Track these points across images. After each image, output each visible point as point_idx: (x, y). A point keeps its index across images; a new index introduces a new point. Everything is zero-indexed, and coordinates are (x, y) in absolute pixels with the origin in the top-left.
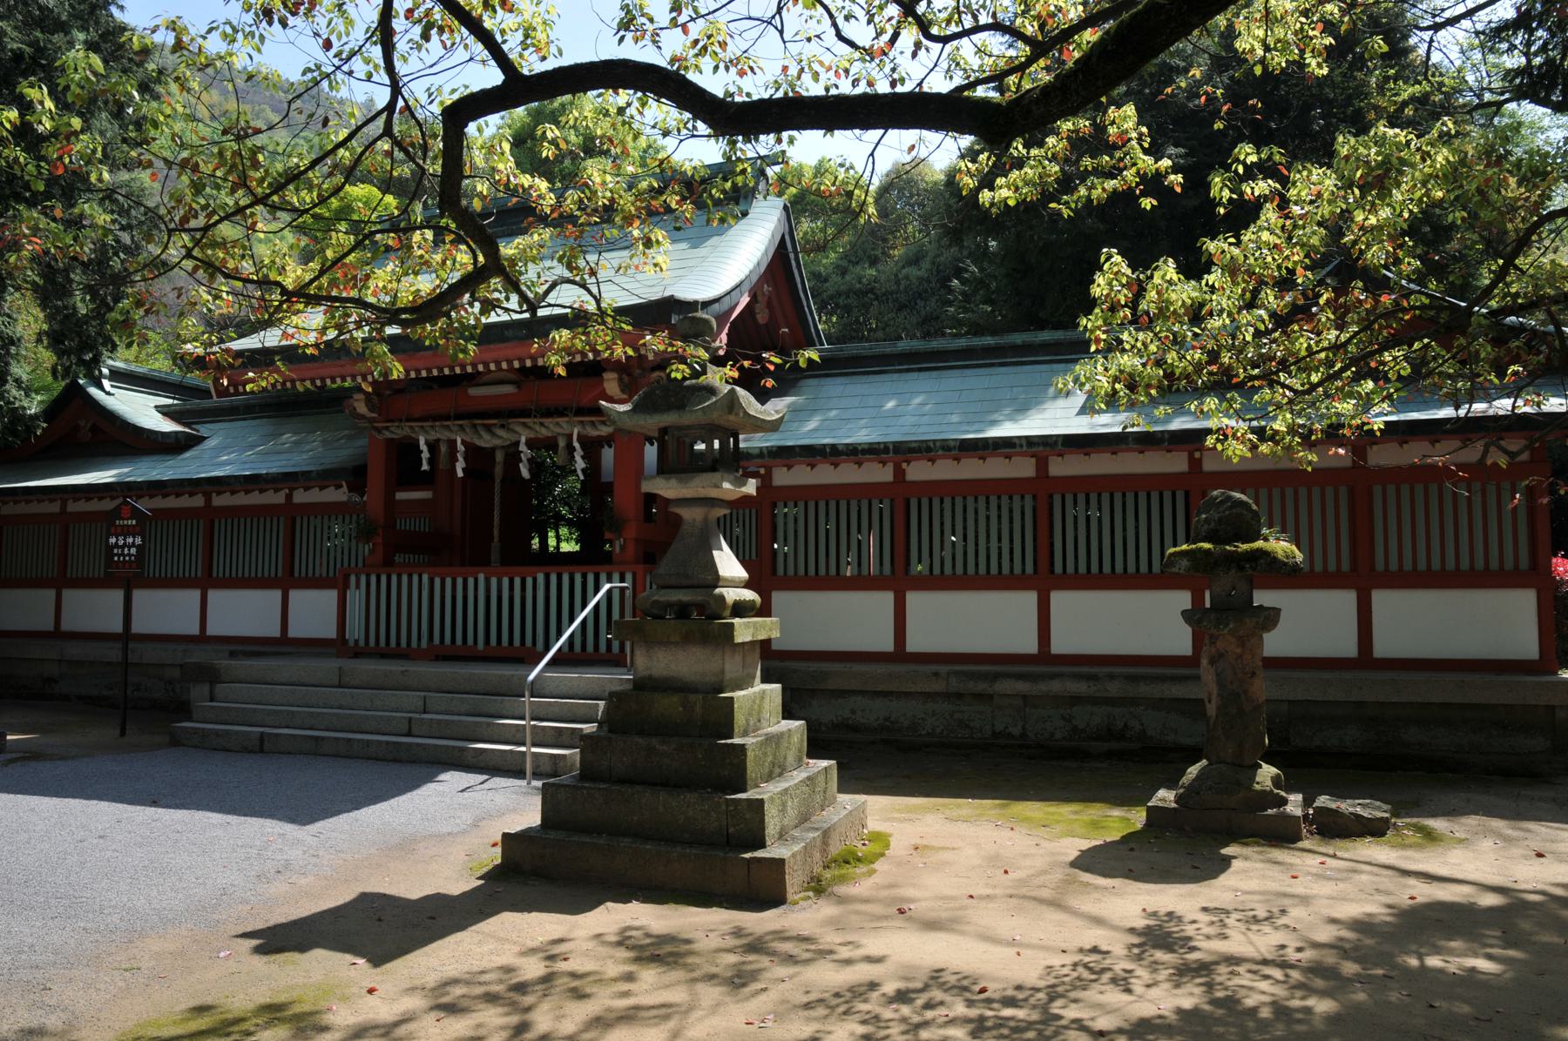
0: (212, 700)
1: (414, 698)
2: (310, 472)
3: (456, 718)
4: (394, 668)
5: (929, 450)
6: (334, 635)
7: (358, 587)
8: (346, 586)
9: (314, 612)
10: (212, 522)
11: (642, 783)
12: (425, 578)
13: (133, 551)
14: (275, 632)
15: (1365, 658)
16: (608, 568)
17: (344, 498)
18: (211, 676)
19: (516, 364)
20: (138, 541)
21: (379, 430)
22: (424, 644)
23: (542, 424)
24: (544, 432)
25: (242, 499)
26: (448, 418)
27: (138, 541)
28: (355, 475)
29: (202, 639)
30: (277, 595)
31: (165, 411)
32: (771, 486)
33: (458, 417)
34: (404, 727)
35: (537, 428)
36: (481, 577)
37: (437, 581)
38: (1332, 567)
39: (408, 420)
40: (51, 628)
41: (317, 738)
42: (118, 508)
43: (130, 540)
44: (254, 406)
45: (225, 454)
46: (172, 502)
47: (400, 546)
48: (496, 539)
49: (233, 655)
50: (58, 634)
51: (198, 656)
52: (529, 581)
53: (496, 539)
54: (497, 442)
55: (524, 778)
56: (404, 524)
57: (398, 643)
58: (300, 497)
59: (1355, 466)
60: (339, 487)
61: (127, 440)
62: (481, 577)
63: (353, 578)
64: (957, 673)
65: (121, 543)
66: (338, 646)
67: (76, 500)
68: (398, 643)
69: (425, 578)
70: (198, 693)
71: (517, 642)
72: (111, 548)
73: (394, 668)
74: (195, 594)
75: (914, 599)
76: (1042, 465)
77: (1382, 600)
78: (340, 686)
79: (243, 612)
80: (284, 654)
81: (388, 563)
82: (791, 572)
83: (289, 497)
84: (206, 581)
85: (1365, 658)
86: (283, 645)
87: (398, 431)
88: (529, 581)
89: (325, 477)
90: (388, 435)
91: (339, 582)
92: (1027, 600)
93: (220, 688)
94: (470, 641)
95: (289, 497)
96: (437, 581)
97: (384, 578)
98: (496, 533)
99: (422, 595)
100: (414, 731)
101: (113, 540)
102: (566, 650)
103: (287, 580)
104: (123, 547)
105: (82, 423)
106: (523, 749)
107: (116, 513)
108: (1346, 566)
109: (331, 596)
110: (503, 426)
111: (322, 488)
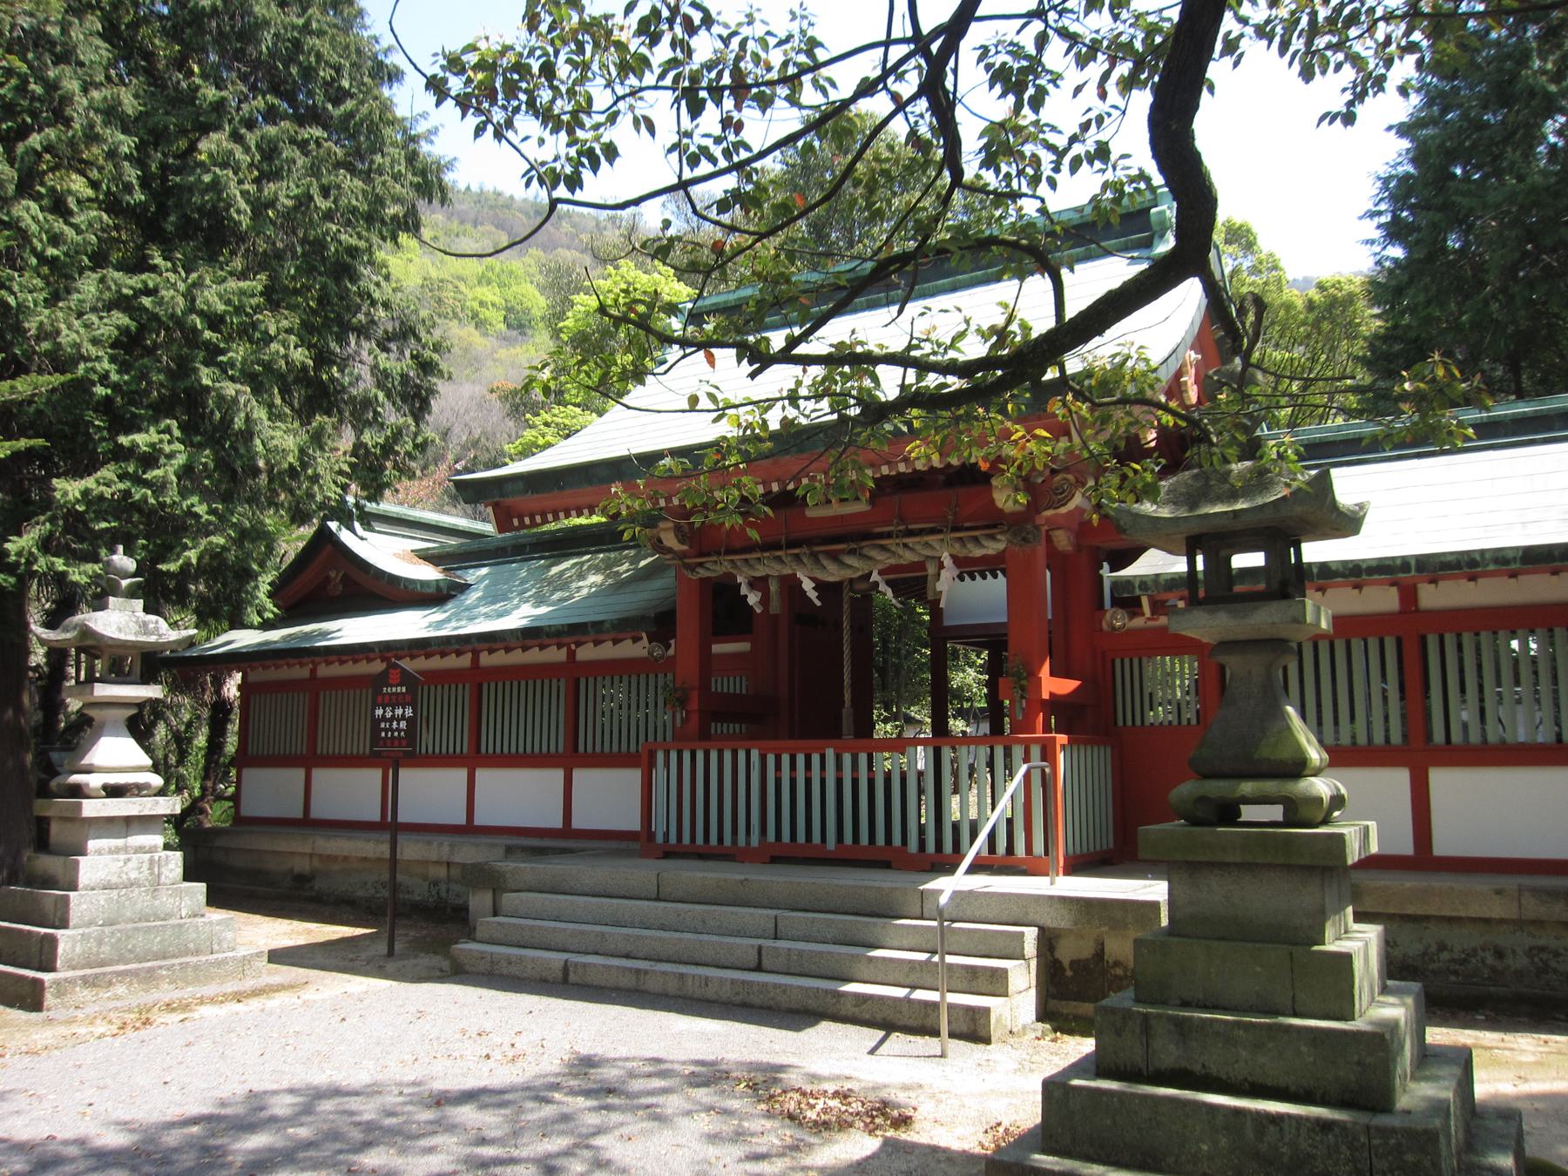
0: (495, 914)
1: (760, 917)
2: (601, 623)
3: (538, 923)
4: (729, 876)
5: (1506, 562)
6: (636, 826)
7: (667, 764)
8: (652, 763)
9: (609, 798)
10: (317, 695)
11: (692, 999)
12: (755, 754)
13: (403, 725)
14: (557, 823)
15: (1423, 858)
16: (706, 744)
17: (645, 653)
18: (493, 882)
19: (775, 487)
20: (409, 712)
21: (692, 568)
22: (755, 840)
23: (905, 545)
24: (909, 557)
25: (517, 657)
26: (778, 547)
27: (409, 712)
28: (661, 624)
29: (469, 829)
30: (558, 775)
31: (426, 557)
32: (1417, 610)
33: (792, 544)
34: (752, 958)
35: (900, 551)
36: (830, 754)
37: (771, 758)
38: (1379, 739)
39: (727, 552)
40: (299, 814)
41: (638, 971)
42: (385, 673)
43: (399, 712)
44: (524, 546)
45: (502, 608)
46: (436, 663)
47: (721, 716)
48: (847, 703)
49: (509, 850)
50: (307, 823)
51: (469, 853)
52: (816, 758)
53: (847, 703)
54: (849, 574)
55: (935, 1033)
56: (724, 684)
57: (720, 839)
58: (586, 653)
59: (1403, 612)
60: (636, 640)
61: (386, 593)
62: (830, 754)
63: (660, 756)
64: (1535, 891)
65: (389, 715)
66: (638, 842)
67: (328, 663)
68: (720, 839)
69: (755, 754)
70: (479, 901)
71: (801, 838)
72: (376, 722)
73: (729, 876)
74: (461, 775)
75: (578, 774)
76: (1409, 595)
77: (1441, 780)
78: (658, 899)
79: (519, 796)
80: (571, 851)
81: (704, 735)
82: (491, 750)
83: (313, 671)
84: (474, 758)
85: (1423, 858)
86: (565, 839)
87: (716, 568)
88: (816, 758)
89: (624, 627)
90: (703, 573)
91: (643, 760)
92: (554, 778)
93: (508, 899)
94: (816, 838)
95: (313, 671)
96: (771, 758)
97: (700, 755)
98: (847, 696)
99: (752, 774)
100: (766, 963)
101: (379, 712)
102: (985, 853)
103: (571, 757)
104: (391, 720)
105: (332, 574)
106: (933, 996)
107: (380, 680)
108: (1396, 738)
109: (634, 776)
110: (852, 552)
111: (616, 642)
